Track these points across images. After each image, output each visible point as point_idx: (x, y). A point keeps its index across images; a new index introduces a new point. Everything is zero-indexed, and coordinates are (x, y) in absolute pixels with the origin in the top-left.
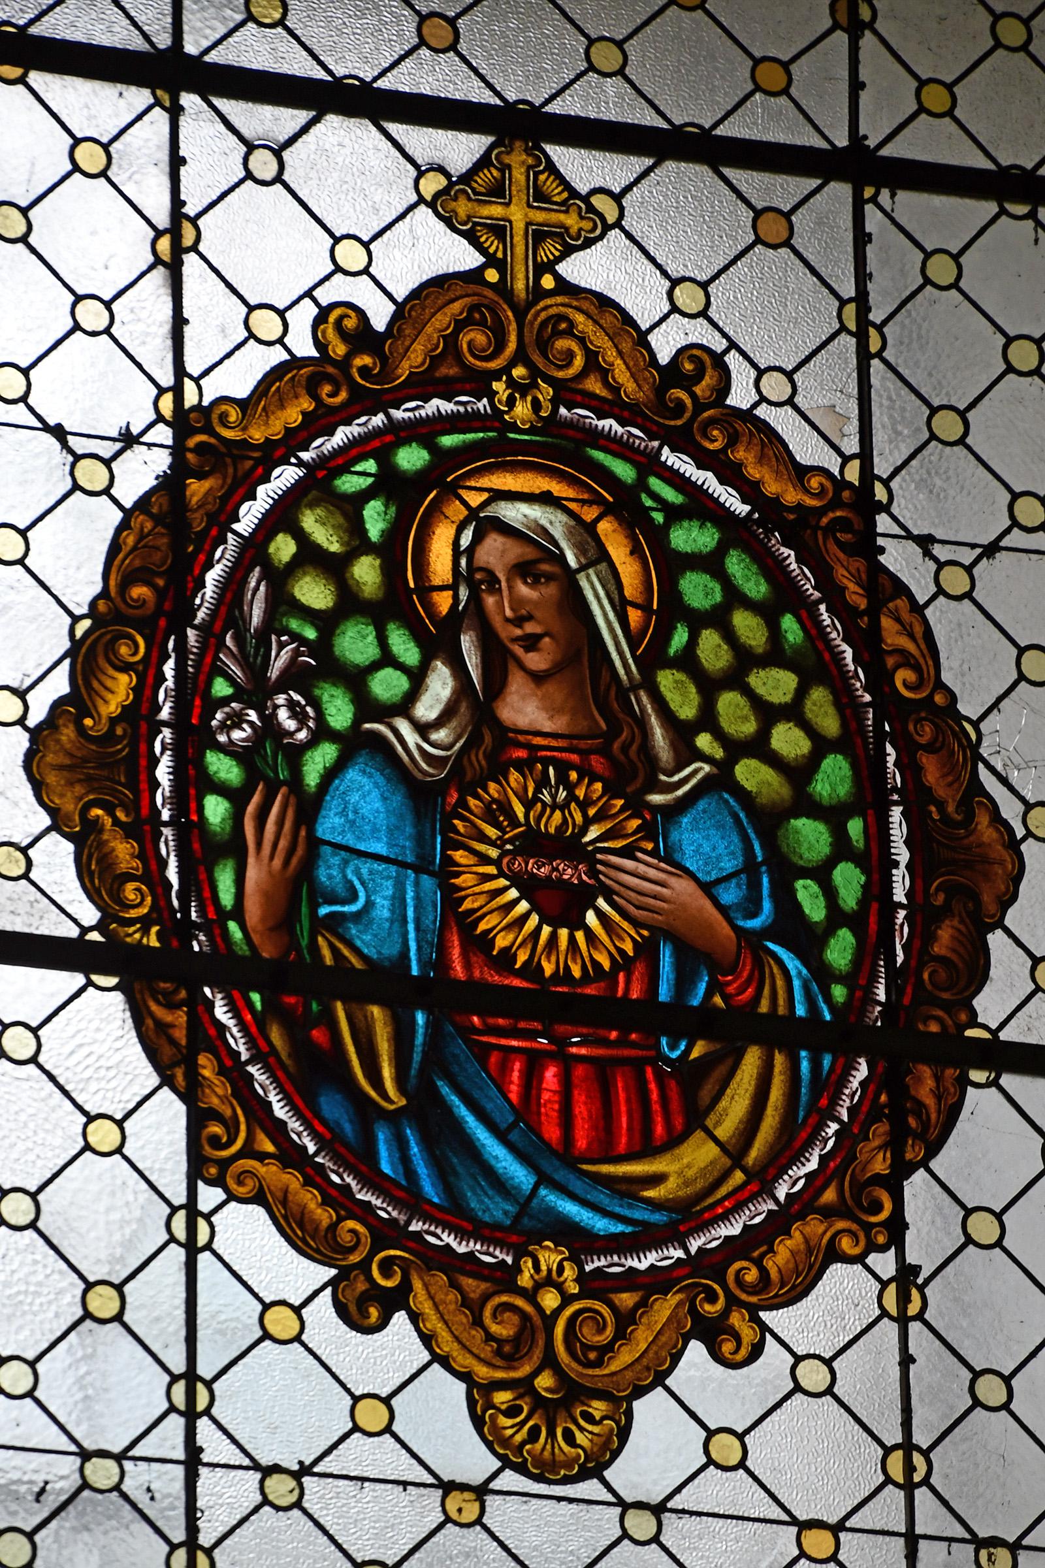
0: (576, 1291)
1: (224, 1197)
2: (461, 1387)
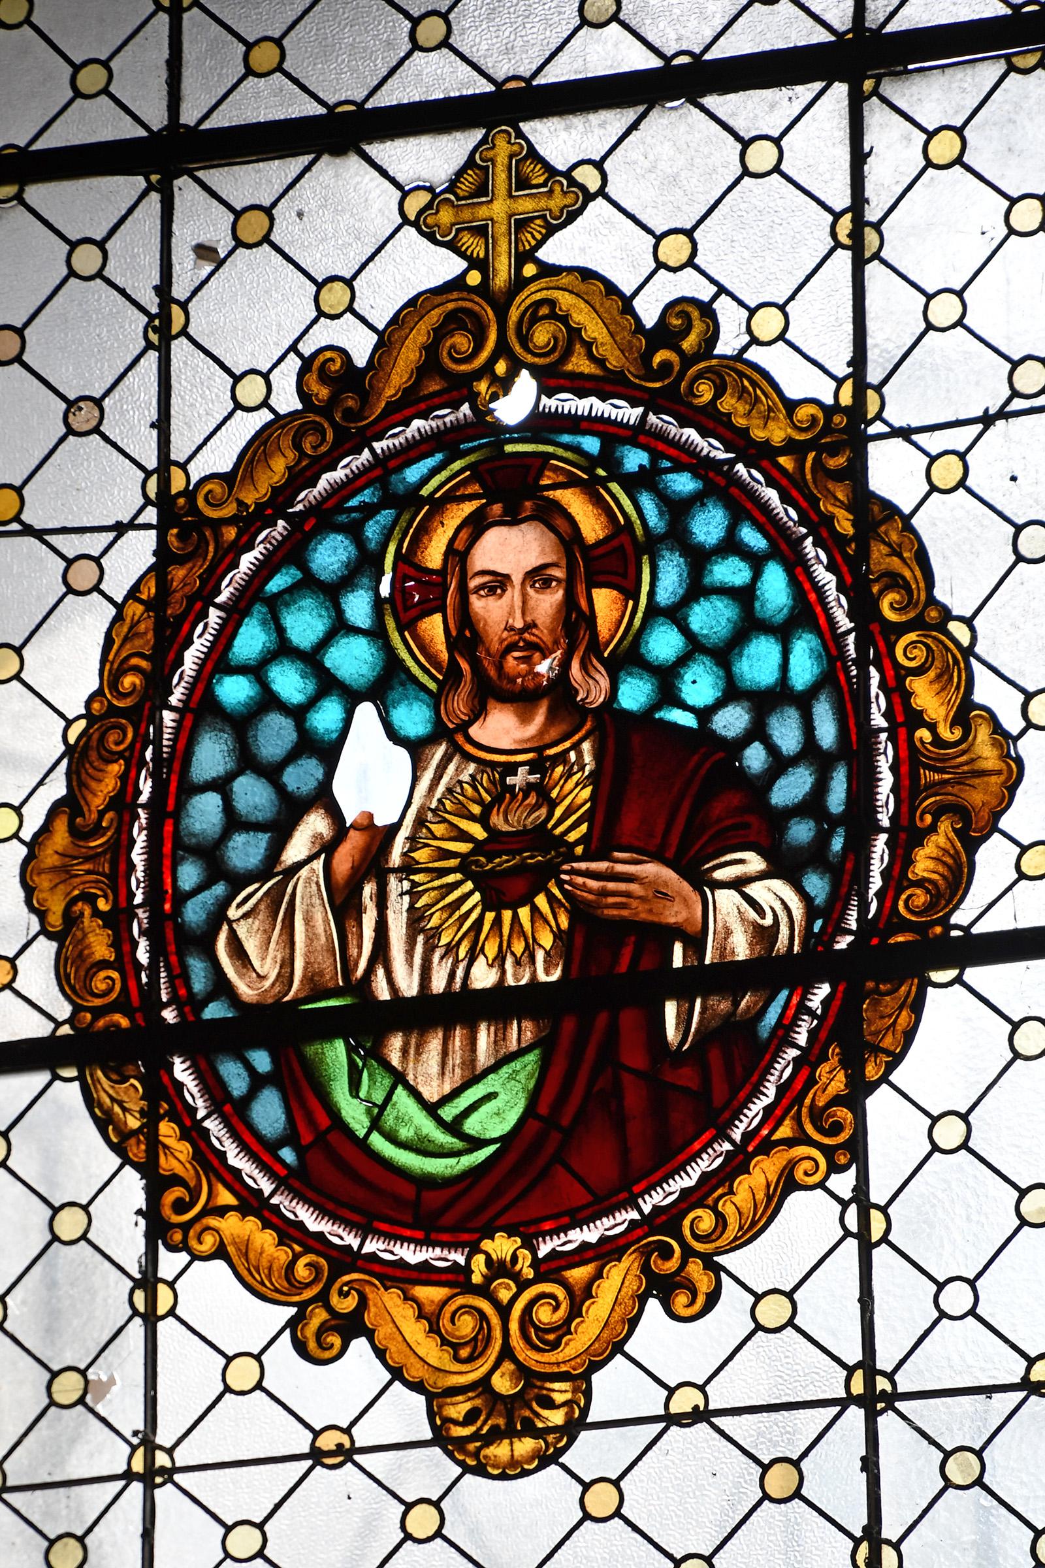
0: (531, 1276)
1: (188, 1258)
2: (420, 1400)
